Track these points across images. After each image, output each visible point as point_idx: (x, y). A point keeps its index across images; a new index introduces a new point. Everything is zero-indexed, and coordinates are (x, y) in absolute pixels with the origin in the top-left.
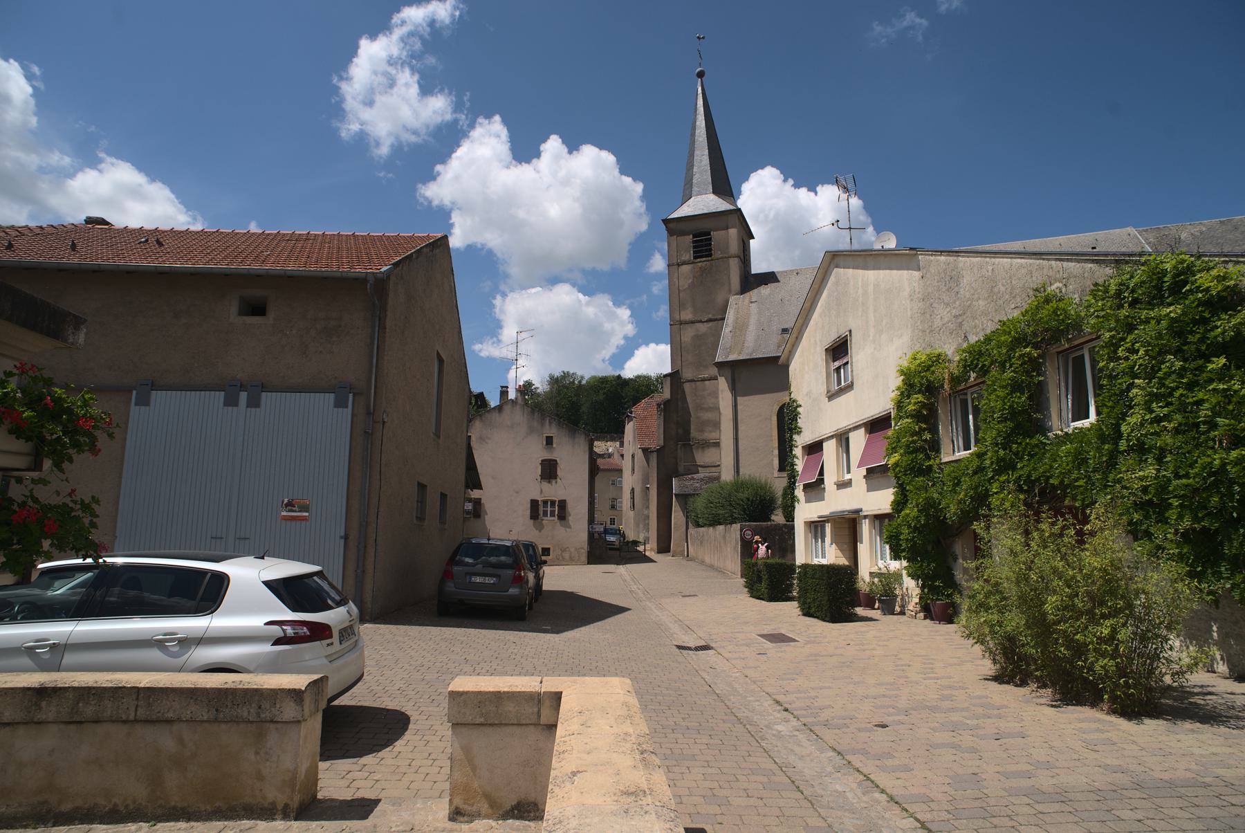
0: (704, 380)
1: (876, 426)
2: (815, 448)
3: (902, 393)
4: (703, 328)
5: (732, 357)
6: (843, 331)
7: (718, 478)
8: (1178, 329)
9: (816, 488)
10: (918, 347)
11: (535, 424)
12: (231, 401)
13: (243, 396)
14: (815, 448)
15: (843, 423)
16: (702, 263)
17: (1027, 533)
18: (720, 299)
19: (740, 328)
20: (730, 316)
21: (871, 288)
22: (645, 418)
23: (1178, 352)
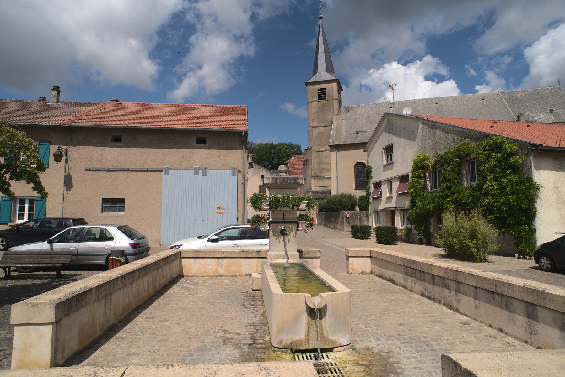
0: (322, 151)
1: (403, 179)
2: (378, 185)
3: (414, 169)
4: (322, 129)
5: (336, 143)
6: (390, 142)
7: (330, 192)
8: (499, 161)
9: (378, 199)
10: (419, 154)
11: (256, 170)
12: (196, 174)
13: (201, 171)
14: (378, 185)
15: (529, 261)
16: (322, 102)
17: (456, 217)
18: (329, 117)
19: (339, 130)
20: (334, 124)
21: (402, 129)
22: (293, 165)
23: (500, 167)
